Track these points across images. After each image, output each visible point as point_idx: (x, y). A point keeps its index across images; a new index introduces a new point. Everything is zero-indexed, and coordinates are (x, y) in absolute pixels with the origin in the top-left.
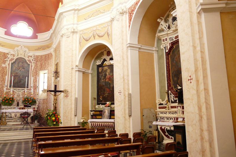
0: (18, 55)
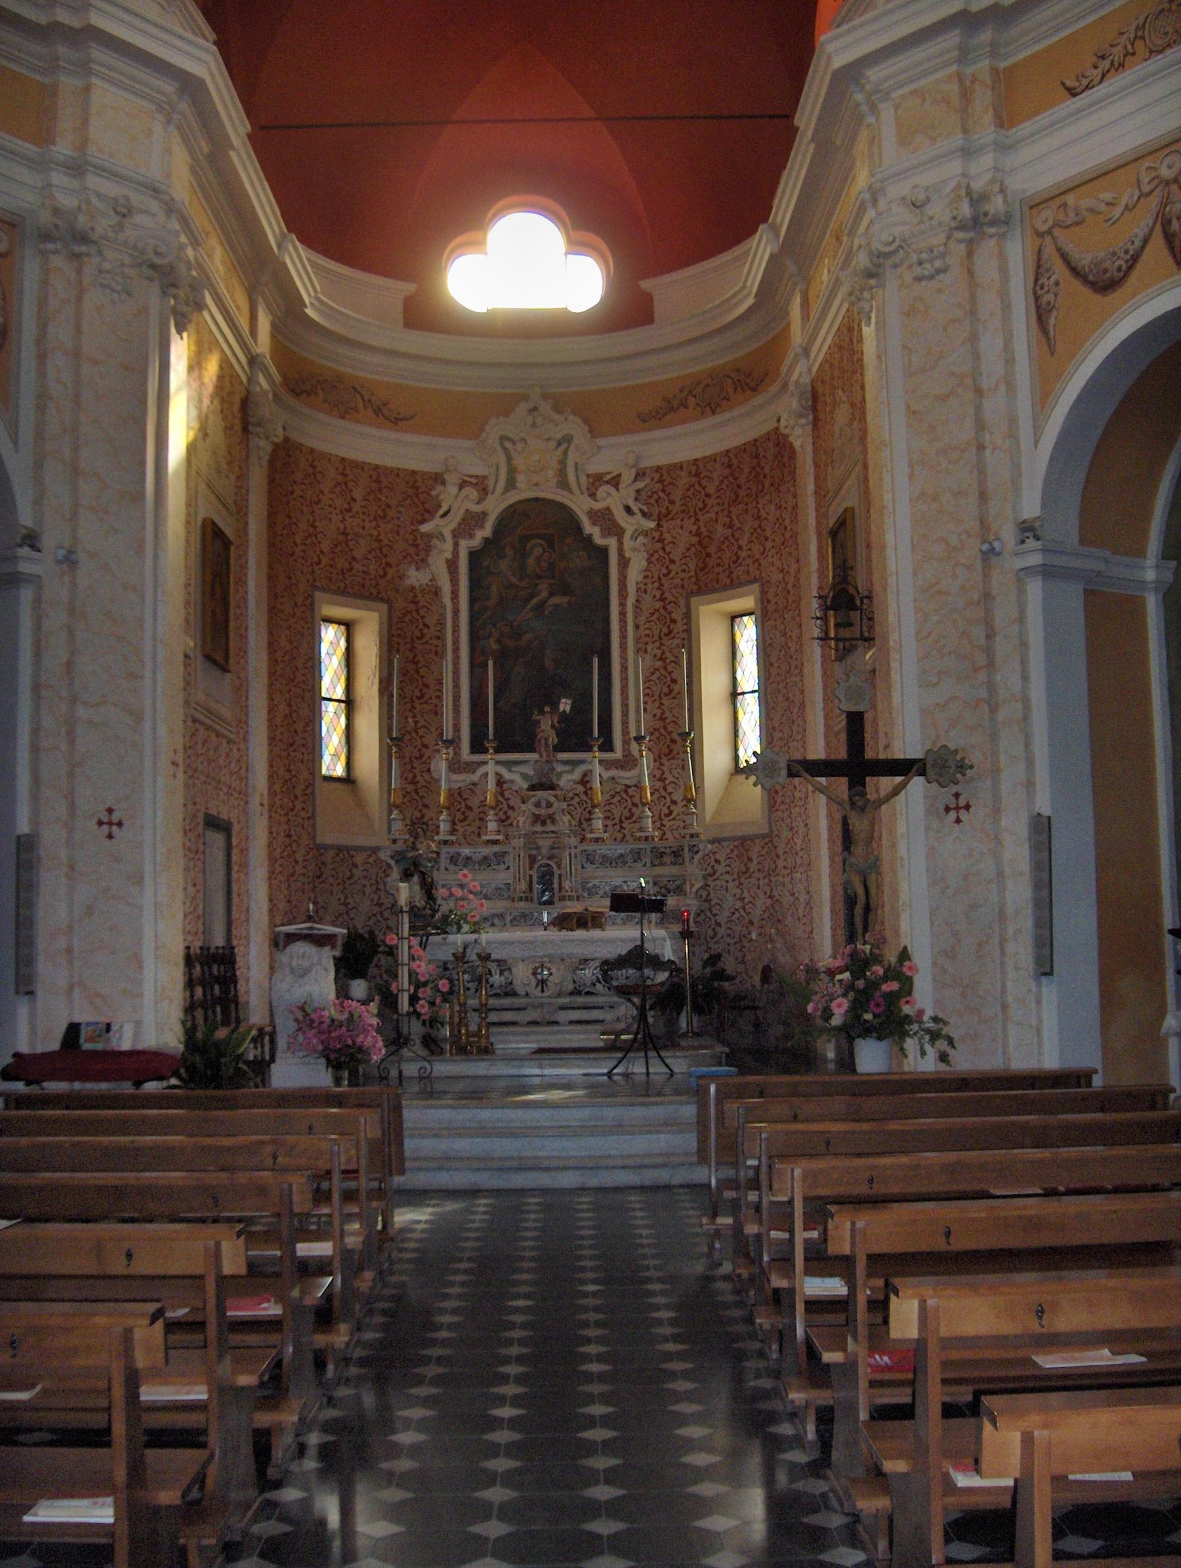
0: (511, 484)
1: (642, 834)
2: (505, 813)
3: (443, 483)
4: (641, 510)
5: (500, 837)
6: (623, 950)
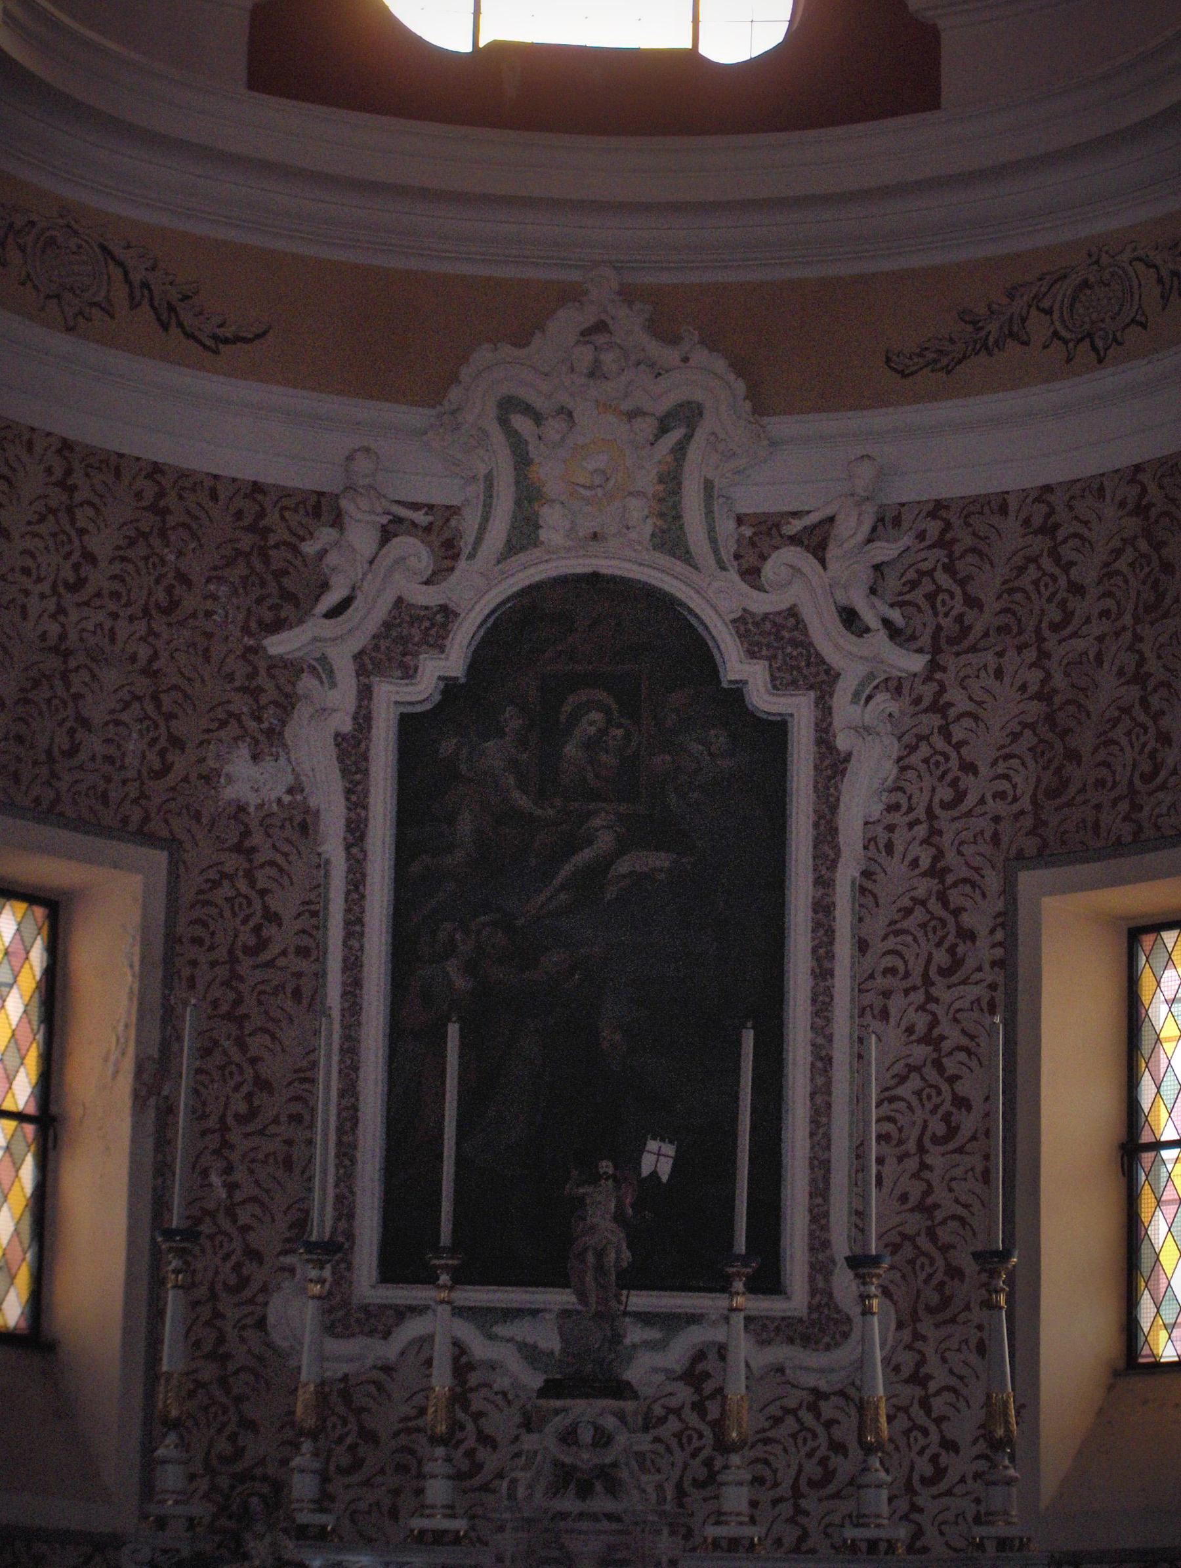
1: (859, 1533)
2: (470, 1454)
3: (338, 522)
4: (887, 623)
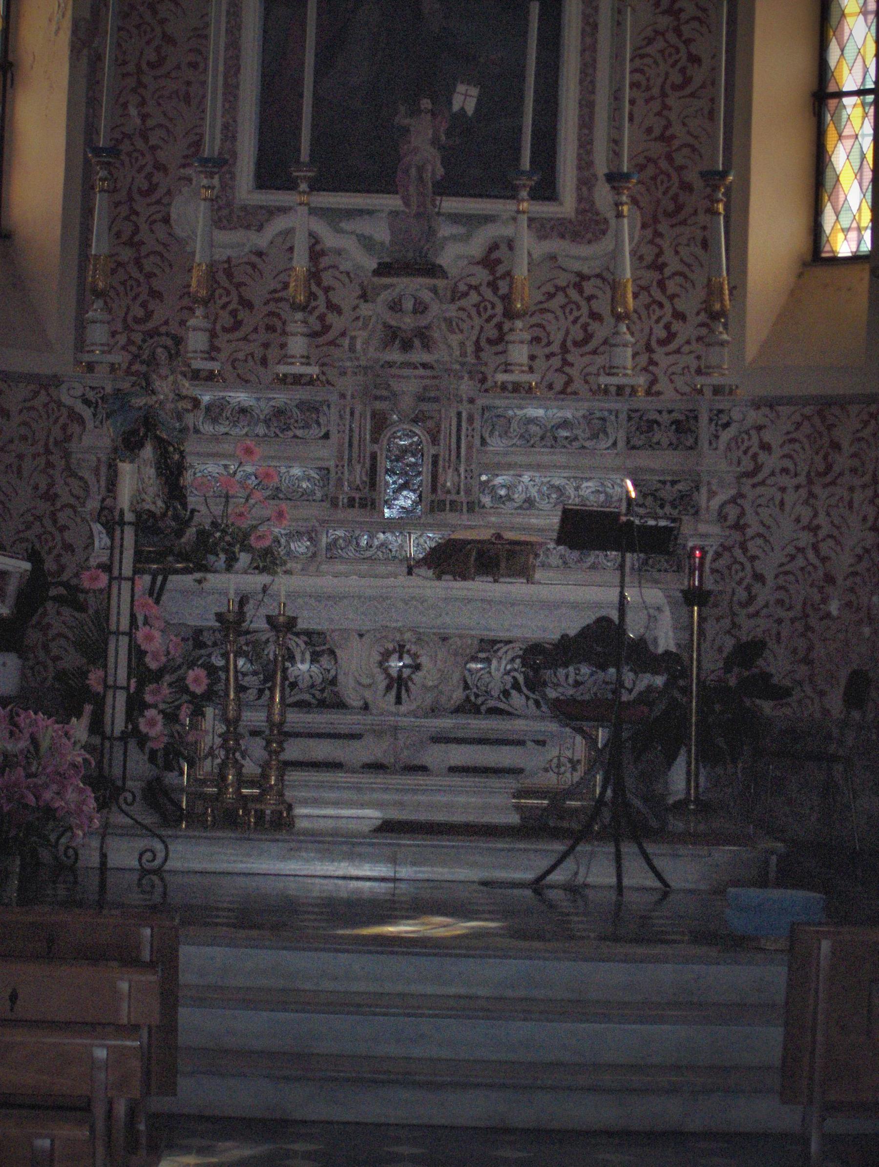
5: (313, 370)
6: (573, 626)
